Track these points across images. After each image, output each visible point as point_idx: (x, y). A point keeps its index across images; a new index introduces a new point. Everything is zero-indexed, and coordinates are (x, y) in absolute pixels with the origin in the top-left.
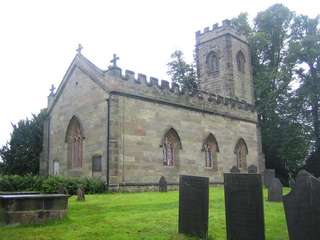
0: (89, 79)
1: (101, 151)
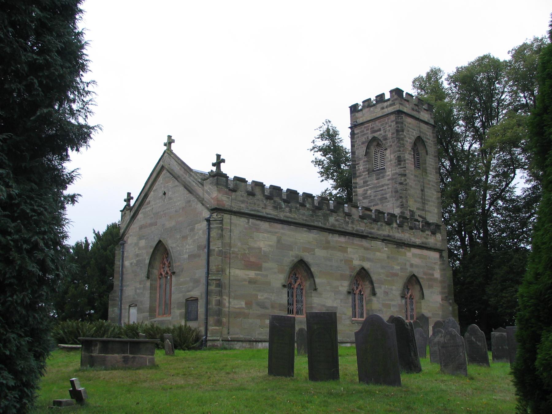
0: (182, 188)
1: (198, 292)
